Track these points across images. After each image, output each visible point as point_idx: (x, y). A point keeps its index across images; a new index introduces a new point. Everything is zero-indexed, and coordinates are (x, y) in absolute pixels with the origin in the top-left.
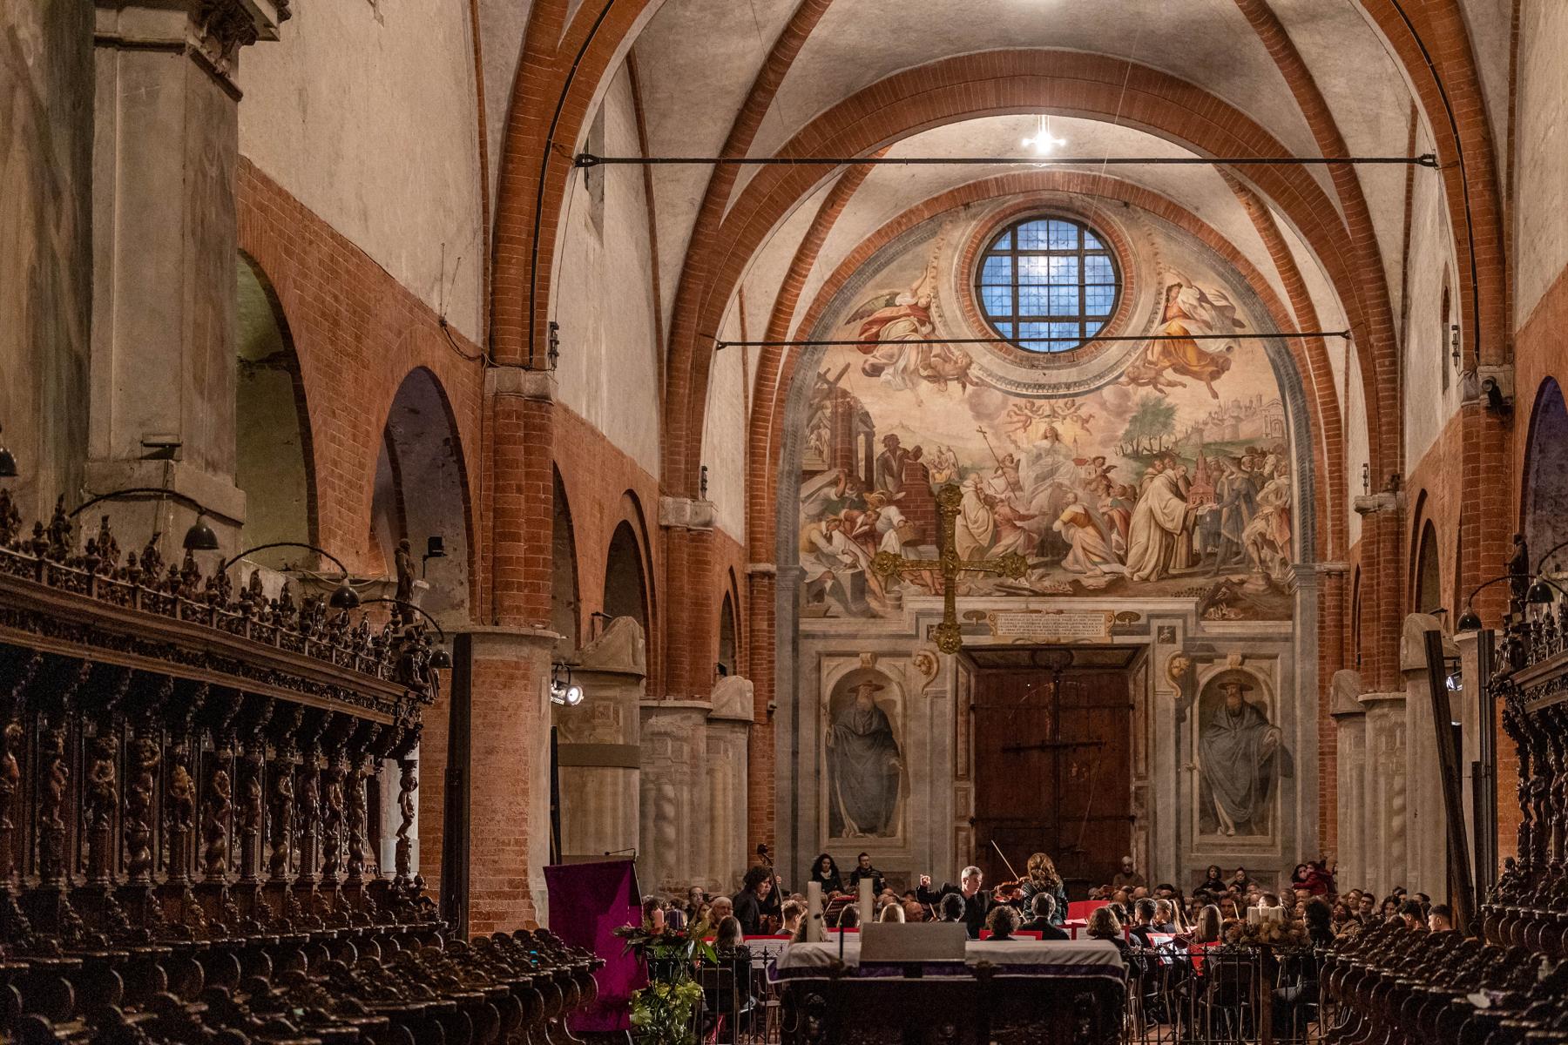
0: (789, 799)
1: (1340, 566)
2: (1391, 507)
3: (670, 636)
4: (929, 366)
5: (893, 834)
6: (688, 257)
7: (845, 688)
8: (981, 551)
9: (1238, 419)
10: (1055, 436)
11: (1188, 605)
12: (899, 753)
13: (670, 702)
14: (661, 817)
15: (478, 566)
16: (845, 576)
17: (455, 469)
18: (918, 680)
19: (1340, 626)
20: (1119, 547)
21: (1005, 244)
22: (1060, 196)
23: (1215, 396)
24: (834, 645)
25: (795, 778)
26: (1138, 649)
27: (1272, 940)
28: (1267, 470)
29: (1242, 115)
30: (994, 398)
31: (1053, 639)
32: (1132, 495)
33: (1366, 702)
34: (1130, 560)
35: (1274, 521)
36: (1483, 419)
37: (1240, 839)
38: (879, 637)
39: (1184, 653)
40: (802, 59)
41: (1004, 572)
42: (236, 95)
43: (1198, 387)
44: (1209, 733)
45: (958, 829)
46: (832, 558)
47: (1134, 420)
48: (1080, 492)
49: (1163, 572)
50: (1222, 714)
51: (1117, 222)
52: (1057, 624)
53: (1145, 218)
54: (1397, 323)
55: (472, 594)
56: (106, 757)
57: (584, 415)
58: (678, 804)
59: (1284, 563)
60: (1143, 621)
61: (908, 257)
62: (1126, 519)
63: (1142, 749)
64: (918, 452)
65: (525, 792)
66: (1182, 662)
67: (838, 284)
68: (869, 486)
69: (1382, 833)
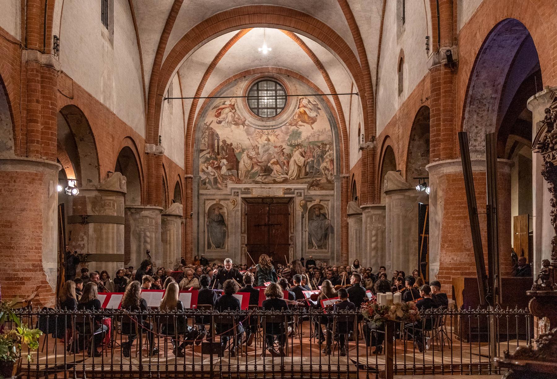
0: (196, 240)
1: (347, 175)
2: (372, 146)
3: (149, 187)
4: (235, 121)
5: (225, 248)
6: (153, 69)
7: (212, 209)
9: (319, 135)
11: (305, 186)
12: (227, 227)
13: (148, 207)
14: (145, 242)
16: (212, 178)
19: (347, 192)
20: (286, 170)
23: (313, 129)
24: (209, 197)
25: (198, 233)
26: (291, 199)
27: (398, 318)
28: (327, 149)
29: (325, 25)
31: (268, 195)
32: (290, 156)
33: (362, 208)
34: (289, 174)
35: (329, 163)
36: (443, 70)
38: (221, 195)
39: (304, 200)
41: (250, 176)
43: (308, 126)
44: (311, 221)
45: (242, 247)
46: (208, 174)
47: (290, 135)
48: (275, 155)
49: (298, 177)
50: (314, 216)
51: (286, 81)
52: (269, 191)
53: (293, 80)
54: (374, 88)
55: (15, 144)
57: (108, 106)
58: (151, 238)
59: (331, 174)
60: (293, 190)
61: (229, 91)
62: (288, 163)
63: (292, 226)
64: (231, 144)
65: (41, 228)
69: (368, 248)
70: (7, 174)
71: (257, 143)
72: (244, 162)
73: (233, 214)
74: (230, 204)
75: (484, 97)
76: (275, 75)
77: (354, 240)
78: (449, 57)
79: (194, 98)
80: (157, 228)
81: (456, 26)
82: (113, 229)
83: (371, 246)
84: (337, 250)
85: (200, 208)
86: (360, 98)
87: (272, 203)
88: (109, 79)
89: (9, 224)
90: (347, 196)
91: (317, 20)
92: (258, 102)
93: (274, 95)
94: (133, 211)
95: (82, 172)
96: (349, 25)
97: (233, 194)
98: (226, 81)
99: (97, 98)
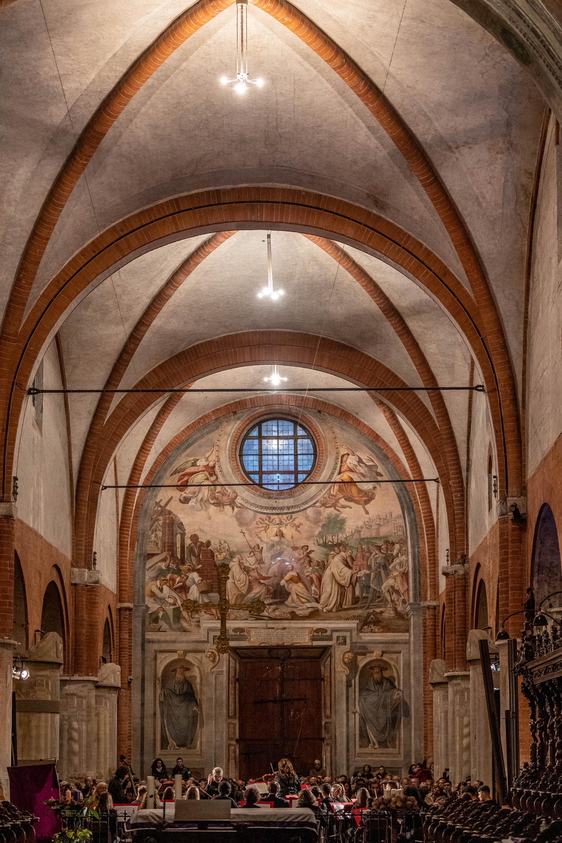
1: (434, 603)
2: (461, 572)
4: (215, 498)
5: (195, 748)
7: (170, 669)
8: (242, 596)
9: (379, 525)
10: (281, 535)
11: (353, 624)
16: (170, 609)
19: (435, 635)
21: (255, 433)
22: (284, 407)
23: (367, 513)
24: (164, 647)
25: (142, 718)
26: (326, 649)
27: (397, 807)
28: (395, 553)
30: (249, 514)
31: (280, 643)
32: (323, 566)
34: (322, 601)
35: (399, 580)
36: (510, 526)
38: (187, 642)
43: (357, 508)
44: (364, 693)
45: (229, 745)
49: (339, 607)
51: (315, 421)
53: (329, 418)
54: (464, 474)
58: (79, 732)
59: (404, 602)
60: (329, 633)
61: (203, 440)
62: (320, 579)
63: (328, 702)
66: (350, 655)
67: (167, 454)
69: (458, 747)
71: (258, 541)
72: (236, 581)
73: (212, 679)
74: (205, 660)
75: (554, 565)
77: (443, 732)
78: (516, 512)
81: (525, 472)
82: (46, 721)
83: (461, 744)
84: (416, 751)
85: (147, 668)
86: (441, 488)
87: (289, 657)
90: (435, 643)
91: (366, 356)
92: (260, 461)
93: (293, 481)
96: (419, 373)
97: (211, 640)
98: (198, 422)
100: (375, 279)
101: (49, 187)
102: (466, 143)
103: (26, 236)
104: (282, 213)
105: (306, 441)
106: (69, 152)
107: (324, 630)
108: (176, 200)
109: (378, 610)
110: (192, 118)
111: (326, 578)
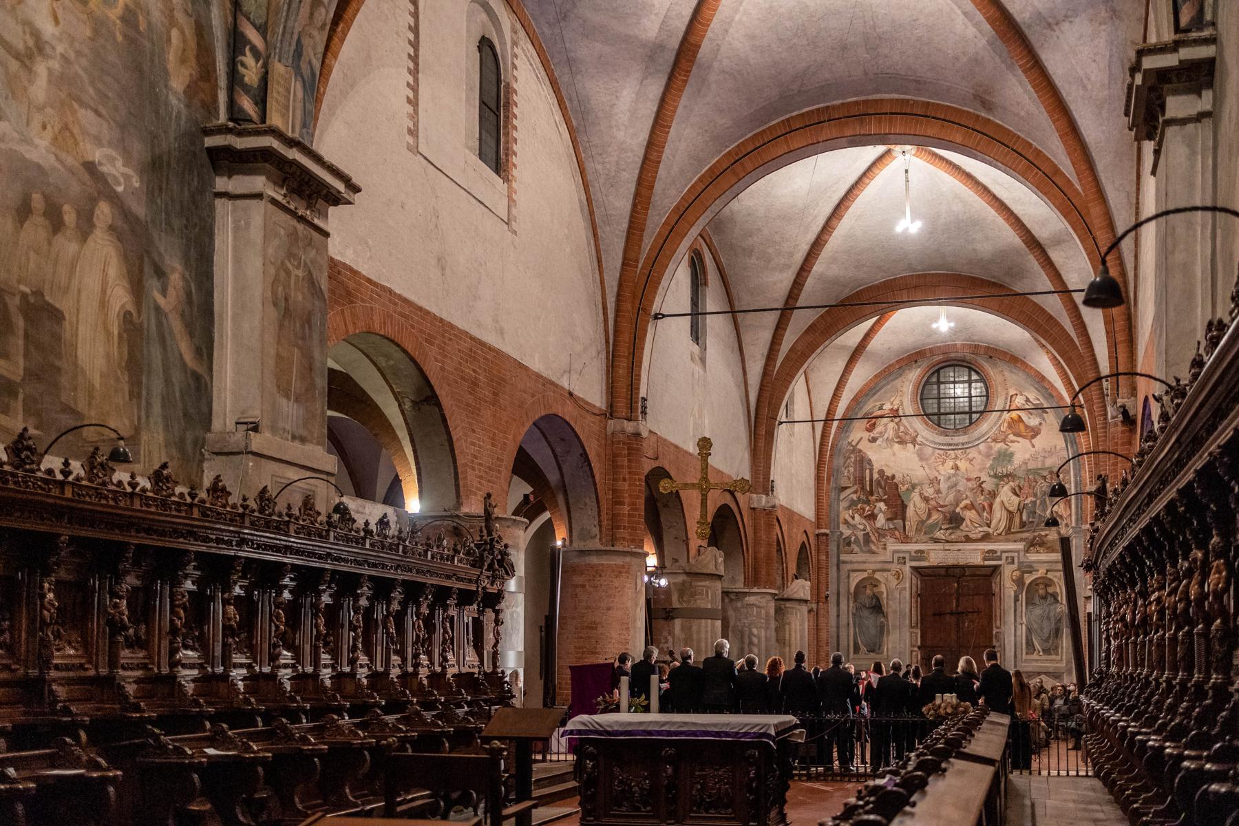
3: (755, 559)
7: (861, 586)
8: (923, 522)
10: (957, 468)
11: (1020, 546)
12: (885, 617)
13: (755, 590)
15: (604, 517)
16: (860, 534)
17: (587, 469)
18: (894, 582)
21: (934, 379)
22: (959, 355)
24: (856, 566)
25: (838, 627)
26: (996, 568)
30: (928, 451)
32: (993, 495)
37: (1045, 657)
40: (810, 282)
41: (925, 528)
42: (326, 235)
43: (1024, 443)
46: (854, 527)
49: (1008, 530)
55: (600, 531)
56: (120, 598)
59: (1067, 525)
62: (991, 506)
64: (893, 477)
65: (628, 629)
66: (1017, 573)
67: (857, 400)
68: (871, 493)
70: (592, 566)
76: (969, 357)
79: (825, 421)
80: (767, 620)
85: (842, 585)
88: (701, 416)
89: (593, 626)
92: (939, 404)
94: (733, 597)
95: (666, 548)
98: (884, 371)
99: (685, 448)
100: (1016, 212)
101: (655, 109)
102: (1066, 17)
103: (639, 161)
104: (890, 123)
105: (979, 385)
106: (669, 70)
107: (994, 552)
108: (788, 120)
109: (1043, 533)
110: (788, 24)
111: (997, 506)
